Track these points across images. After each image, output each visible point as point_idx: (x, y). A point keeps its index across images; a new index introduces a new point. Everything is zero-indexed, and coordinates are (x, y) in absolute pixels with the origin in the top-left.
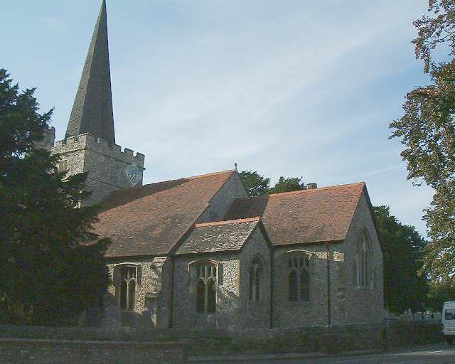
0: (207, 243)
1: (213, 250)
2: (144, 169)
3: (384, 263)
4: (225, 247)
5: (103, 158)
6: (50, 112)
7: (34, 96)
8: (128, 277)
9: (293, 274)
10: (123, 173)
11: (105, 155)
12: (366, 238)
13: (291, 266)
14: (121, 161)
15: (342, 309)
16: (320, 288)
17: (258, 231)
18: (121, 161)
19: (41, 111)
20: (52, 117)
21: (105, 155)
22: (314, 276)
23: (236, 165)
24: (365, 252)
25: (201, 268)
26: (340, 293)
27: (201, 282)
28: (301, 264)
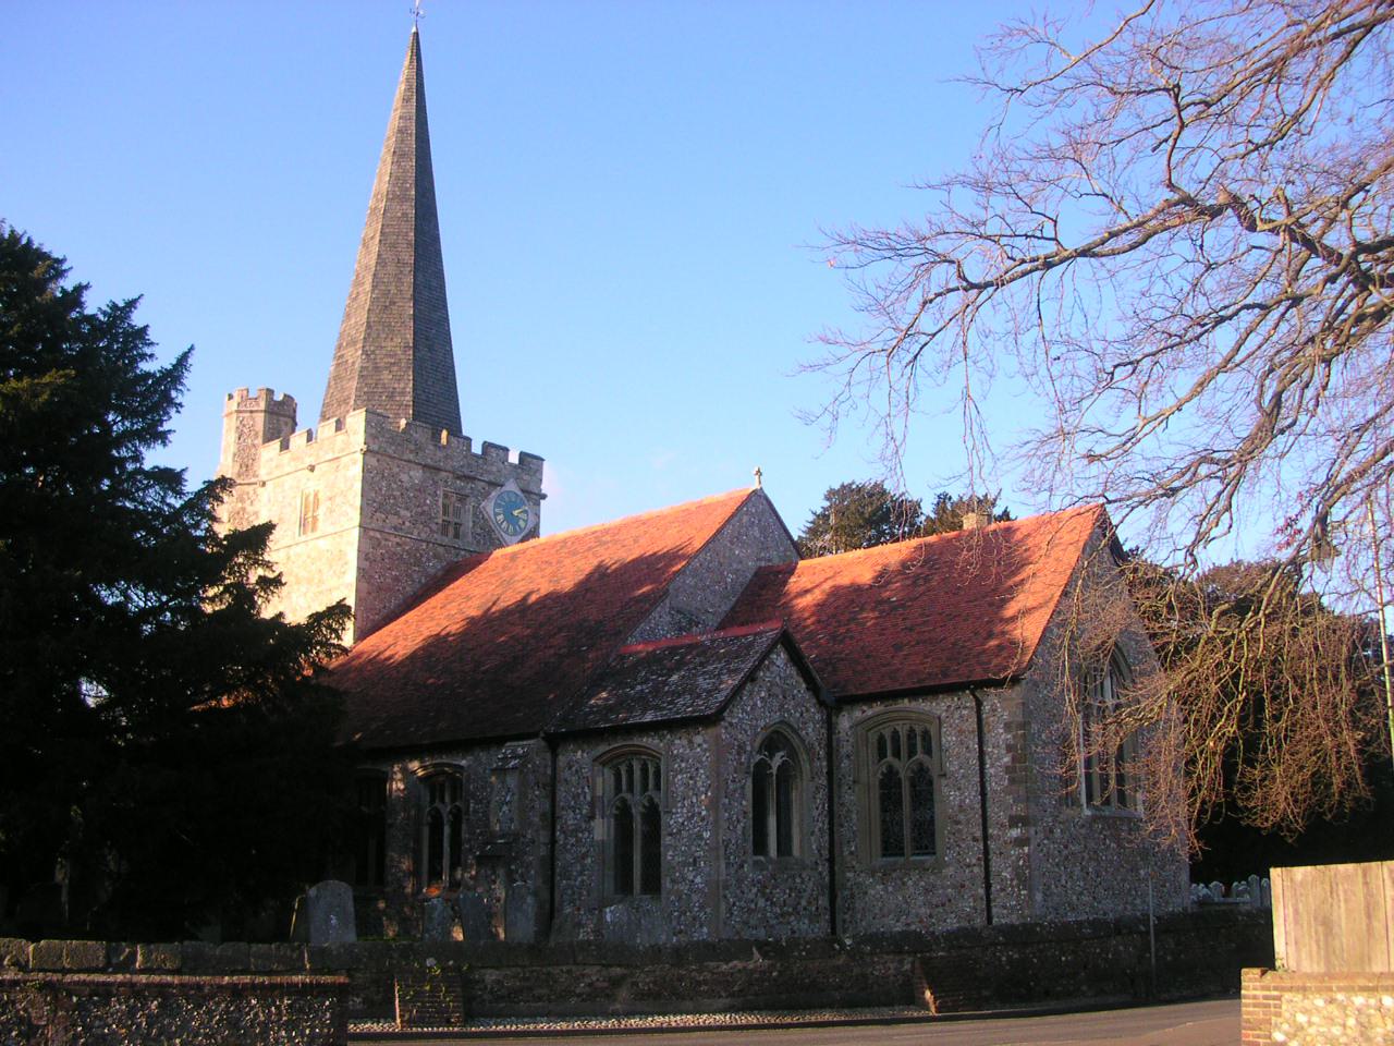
1: (648, 718)
2: (544, 497)
5: (417, 474)
6: (182, 362)
7: (138, 319)
8: (447, 799)
9: (890, 782)
10: (478, 514)
13: (882, 754)
14: (473, 479)
15: (1023, 879)
16: (961, 817)
17: (780, 658)
18: (473, 479)
19: (158, 361)
20: (190, 379)
22: (944, 782)
23: (759, 473)
26: (1015, 832)
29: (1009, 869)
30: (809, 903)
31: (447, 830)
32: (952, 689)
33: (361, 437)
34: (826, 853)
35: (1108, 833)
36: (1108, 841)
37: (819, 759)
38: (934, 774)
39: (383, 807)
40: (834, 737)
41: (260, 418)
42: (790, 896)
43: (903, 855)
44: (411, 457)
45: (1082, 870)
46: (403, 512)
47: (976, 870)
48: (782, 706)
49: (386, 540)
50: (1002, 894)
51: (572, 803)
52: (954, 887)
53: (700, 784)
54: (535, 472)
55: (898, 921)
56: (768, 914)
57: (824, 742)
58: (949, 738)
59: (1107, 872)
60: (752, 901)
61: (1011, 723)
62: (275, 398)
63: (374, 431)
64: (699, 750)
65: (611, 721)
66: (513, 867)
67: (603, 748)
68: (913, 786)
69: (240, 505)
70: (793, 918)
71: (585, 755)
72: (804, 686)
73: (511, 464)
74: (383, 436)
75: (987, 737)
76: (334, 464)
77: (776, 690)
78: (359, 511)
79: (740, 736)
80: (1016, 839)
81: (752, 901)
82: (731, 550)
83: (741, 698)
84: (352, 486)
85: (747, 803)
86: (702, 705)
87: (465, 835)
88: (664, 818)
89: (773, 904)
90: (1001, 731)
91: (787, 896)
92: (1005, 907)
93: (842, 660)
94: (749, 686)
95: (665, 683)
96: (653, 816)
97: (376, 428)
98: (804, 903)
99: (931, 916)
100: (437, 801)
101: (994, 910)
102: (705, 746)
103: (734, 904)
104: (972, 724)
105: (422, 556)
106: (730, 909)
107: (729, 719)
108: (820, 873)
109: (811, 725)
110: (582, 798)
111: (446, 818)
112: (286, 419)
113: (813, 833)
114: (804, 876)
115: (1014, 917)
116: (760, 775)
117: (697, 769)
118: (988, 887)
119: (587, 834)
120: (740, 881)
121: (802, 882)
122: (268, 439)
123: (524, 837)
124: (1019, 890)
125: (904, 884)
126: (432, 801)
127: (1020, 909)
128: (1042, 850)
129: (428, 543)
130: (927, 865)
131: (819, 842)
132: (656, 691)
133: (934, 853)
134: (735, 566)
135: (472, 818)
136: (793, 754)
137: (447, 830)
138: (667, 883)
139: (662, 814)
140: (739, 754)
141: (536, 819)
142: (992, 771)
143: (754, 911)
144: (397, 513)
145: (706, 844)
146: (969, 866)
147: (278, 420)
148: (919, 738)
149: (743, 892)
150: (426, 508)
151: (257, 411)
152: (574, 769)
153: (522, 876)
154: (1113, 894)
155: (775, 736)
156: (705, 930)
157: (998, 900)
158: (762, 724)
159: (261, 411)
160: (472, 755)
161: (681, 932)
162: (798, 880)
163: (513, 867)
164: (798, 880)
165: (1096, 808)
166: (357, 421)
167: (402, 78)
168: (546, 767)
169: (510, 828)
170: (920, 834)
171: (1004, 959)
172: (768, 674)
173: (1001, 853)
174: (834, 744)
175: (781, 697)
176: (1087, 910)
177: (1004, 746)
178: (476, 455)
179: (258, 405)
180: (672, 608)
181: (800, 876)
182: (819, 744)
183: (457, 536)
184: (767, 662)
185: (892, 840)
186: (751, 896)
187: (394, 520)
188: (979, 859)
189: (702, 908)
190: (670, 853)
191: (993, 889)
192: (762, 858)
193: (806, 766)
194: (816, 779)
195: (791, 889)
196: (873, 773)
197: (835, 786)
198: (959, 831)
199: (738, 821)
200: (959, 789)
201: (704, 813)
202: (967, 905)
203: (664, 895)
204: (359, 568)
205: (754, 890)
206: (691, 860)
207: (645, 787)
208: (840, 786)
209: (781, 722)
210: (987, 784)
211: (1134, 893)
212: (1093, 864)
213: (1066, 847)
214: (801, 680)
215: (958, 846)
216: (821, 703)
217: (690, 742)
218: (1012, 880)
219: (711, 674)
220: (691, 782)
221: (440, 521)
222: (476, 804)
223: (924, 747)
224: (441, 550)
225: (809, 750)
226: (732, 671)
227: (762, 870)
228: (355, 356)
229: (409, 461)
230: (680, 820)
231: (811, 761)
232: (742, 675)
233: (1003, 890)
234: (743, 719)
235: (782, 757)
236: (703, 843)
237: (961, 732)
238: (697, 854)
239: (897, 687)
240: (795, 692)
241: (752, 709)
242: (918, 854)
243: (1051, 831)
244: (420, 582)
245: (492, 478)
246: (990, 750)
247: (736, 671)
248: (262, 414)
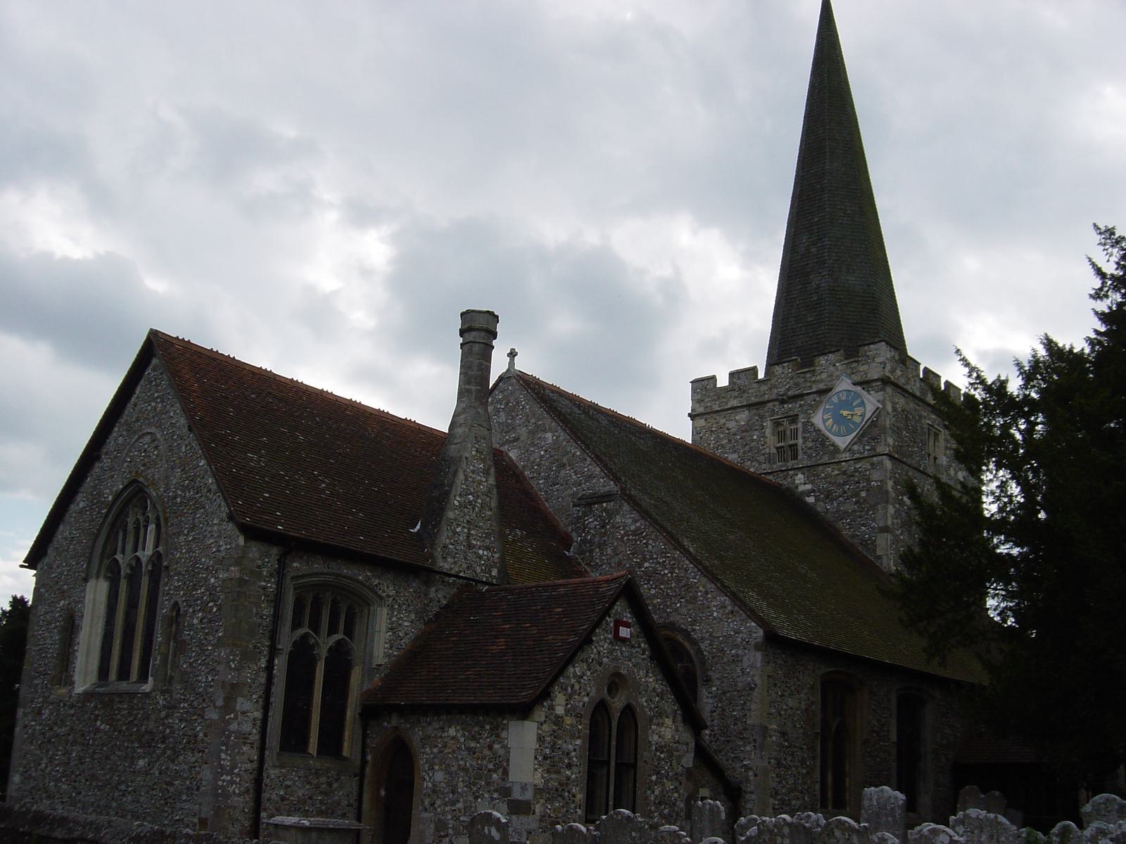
8: (129, 547)
11: (749, 406)
21: (749, 406)
137: (145, 581)
245: (822, 386)
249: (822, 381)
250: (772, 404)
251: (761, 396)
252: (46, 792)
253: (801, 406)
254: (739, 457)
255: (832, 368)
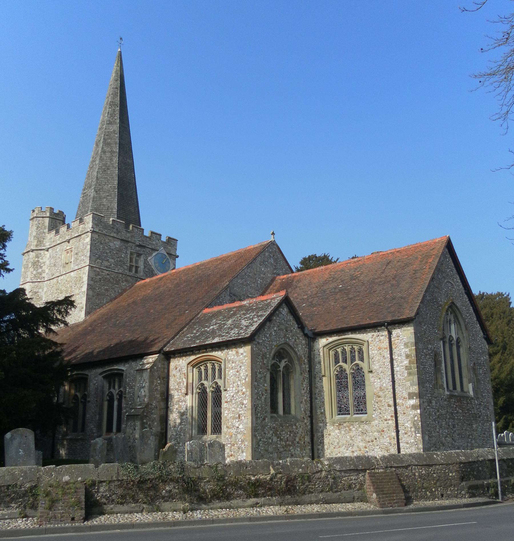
0: (213, 331)
1: (216, 340)
3: (220, 406)
4: (233, 335)
5: (118, 243)
8: (116, 387)
10: (146, 262)
11: (122, 240)
12: (456, 317)
13: (337, 361)
14: (144, 247)
16: (381, 394)
17: (285, 310)
21: (122, 240)
22: (371, 375)
24: (454, 342)
25: (203, 368)
27: (342, 371)
28: (353, 359)
29: (409, 422)
30: (300, 439)
31: (116, 403)
32: (374, 327)
33: (90, 225)
34: (308, 413)
35: (457, 404)
36: (457, 409)
37: (304, 364)
38: (366, 370)
39: (86, 393)
40: (312, 353)
41: (47, 220)
42: (290, 435)
43: (349, 414)
44: (115, 235)
45: (446, 424)
46: (110, 260)
47: (390, 422)
48: (285, 336)
49: (102, 272)
50: (406, 436)
51: (177, 387)
52: (378, 432)
53: (242, 374)
54: (173, 246)
55: (347, 450)
56: (279, 446)
57: (307, 355)
58: (373, 352)
59: (458, 425)
60: (270, 438)
61: (408, 343)
62: (54, 212)
63: (96, 222)
64: (241, 356)
65: (197, 343)
66: (145, 421)
67: (193, 358)
68: (354, 377)
69: (37, 259)
70: (291, 448)
71: (184, 362)
72: (296, 326)
73: (162, 242)
74: (101, 225)
75: (394, 351)
76: (78, 239)
77: (282, 327)
78: (89, 258)
79: (263, 349)
80: (413, 406)
81: (270, 438)
82: (260, 268)
83: (264, 330)
84: (86, 247)
85: (267, 385)
86: (243, 333)
87: (124, 405)
88: (223, 393)
89: (281, 440)
90: (403, 347)
91: (288, 436)
92: (407, 443)
93: (316, 315)
94: (268, 324)
95: (225, 324)
96: (218, 392)
97: (98, 220)
98: (297, 440)
99: (366, 447)
100: (112, 388)
101: (401, 445)
102: (245, 354)
103: (260, 440)
104: (386, 344)
105: (119, 280)
106: (258, 443)
107: (258, 340)
108: (306, 424)
109: (300, 346)
110: (182, 384)
111: (116, 397)
112: (60, 221)
113: (301, 402)
114: (297, 425)
115: (413, 448)
116: (274, 370)
117: (240, 367)
118: (398, 432)
119: (184, 403)
120: (263, 427)
121: (297, 429)
122: (50, 230)
123: (152, 405)
124: (416, 434)
125: (350, 430)
126: (110, 388)
127: (416, 445)
128: (427, 412)
129: (122, 274)
130: (363, 420)
131: (305, 407)
132: (220, 328)
133: (366, 413)
134: (262, 275)
135: (127, 396)
136: (291, 361)
137: (116, 403)
138: (224, 429)
139: (222, 391)
140: (262, 359)
141: (158, 396)
142: (398, 369)
143: (271, 444)
144: (107, 260)
145: (245, 407)
146: (386, 420)
147: (56, 222)
148: (357, 353)
149: (265, 433)
150: (121, 259)
151: (45, 217)
152: (178, 369)
153: (150, 425)
154: (462, 437)
155: (281, 351)
156: (244, 454)
157: (403, 439)
158: (275, 343)
159: (47, 217)
160: (128, 364)
161: (231, 455)
162: (294, 427)
163: (145, 421)
164: (294, 427)
165: (450, 391)
166: (89, 219)
167: (114, 71)
168: (164, 368)
169: (144, 400)
170: (358, 403)
171: (417, 474)
172: (278, 319)
173: (404, 413)
174: (312, 357)
175: (284, 330)
176: (450, 446)
177: (404, 355)
178: (146, 237)
179: (46, 214)
180: (230, 293)
181: (295, 425)
182: (304, 356)
183: (136, 272)
184: (277, 312)
185: (343, 406)
186: (269, 435)
187: (106, 263)
188: (392, 416)
189: (242, 441)
190: (226, 412)
191: (400, 433)
192: (275, 415)
193: (298, 367)
194: (303, 374)
195: (290, 432)
196: (333, 370)
197: (313, 379)
198: (381, 401)
199: (263, 395)
200: (380, 379)
201: (244, 390)
202: (386, 441)
203: (223, 434)
204: (88, 284)
205: (271, 432)
206: (237, 416)
207: (214, 377)
208: (315, 378)
209: (285, 343)
210: (395, 376)
211: (471, 437)
212: (451, 420)
213: (438, 411)
214: (295, 323)
215: (380, 409)
216: (306, 335)
217: (237, 352)
218: (411, 428)
219: (248, 319)
220: (237, 374)
221: (128, 265)
222: (130, 389)
223: (359, 357)
224: (129, 278)
225: (299, 359)
226: (260, 316)
227: (275, 421)
228: (92, 193)
229: (113, 237)
230: (232, 394)
231: (300, 365)
232: (265, 317)
233: (406, 433)
234: (265, 340)
235: (285, 362)
236: (243, 406)
237: (380, 349)
238: (240, 413)
239: (344, 326)
240: (292, 328)
241: (269, 335)
242: (357, 414)
243: (431, 402)
244: (118, 292)
245: (153, 247)
246: (396, 357)
247: (261, 316)
248: (48, 219)
249: (153, 244)
250: (131, 244)
251: (127, 238)
252: (340, 407)
253: (144, 251)
254: (115, 262)
255: (157, 241)
